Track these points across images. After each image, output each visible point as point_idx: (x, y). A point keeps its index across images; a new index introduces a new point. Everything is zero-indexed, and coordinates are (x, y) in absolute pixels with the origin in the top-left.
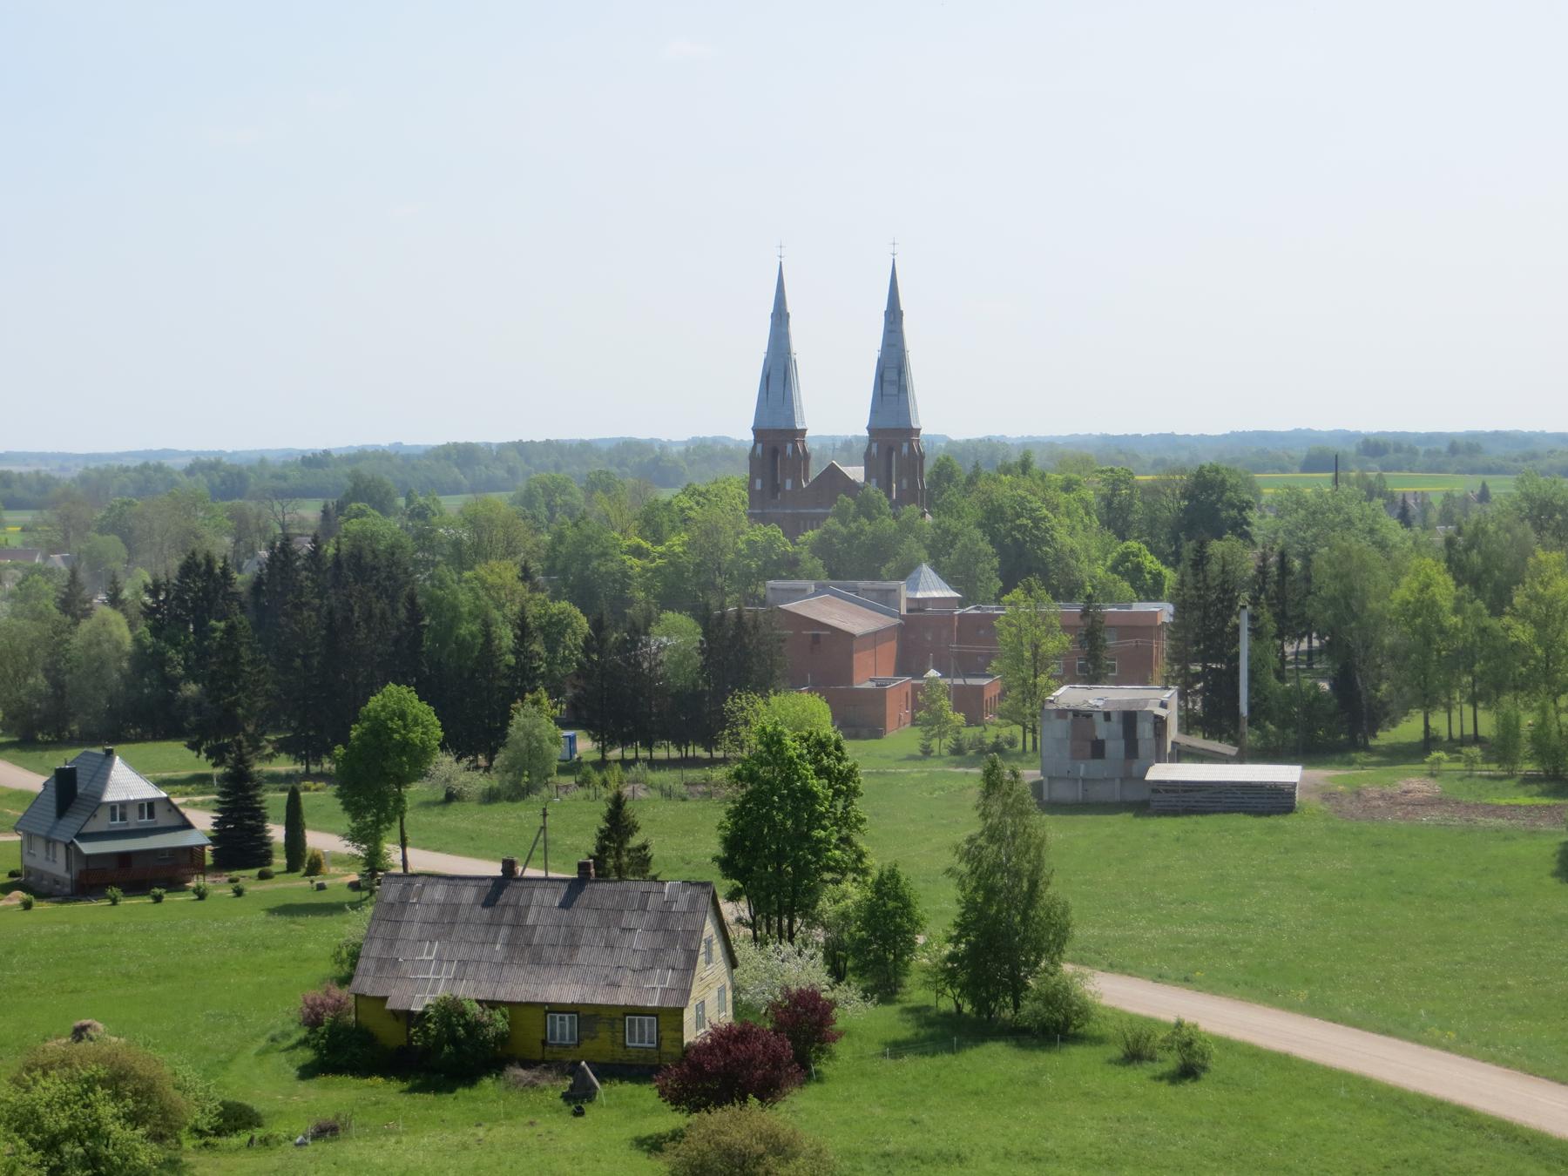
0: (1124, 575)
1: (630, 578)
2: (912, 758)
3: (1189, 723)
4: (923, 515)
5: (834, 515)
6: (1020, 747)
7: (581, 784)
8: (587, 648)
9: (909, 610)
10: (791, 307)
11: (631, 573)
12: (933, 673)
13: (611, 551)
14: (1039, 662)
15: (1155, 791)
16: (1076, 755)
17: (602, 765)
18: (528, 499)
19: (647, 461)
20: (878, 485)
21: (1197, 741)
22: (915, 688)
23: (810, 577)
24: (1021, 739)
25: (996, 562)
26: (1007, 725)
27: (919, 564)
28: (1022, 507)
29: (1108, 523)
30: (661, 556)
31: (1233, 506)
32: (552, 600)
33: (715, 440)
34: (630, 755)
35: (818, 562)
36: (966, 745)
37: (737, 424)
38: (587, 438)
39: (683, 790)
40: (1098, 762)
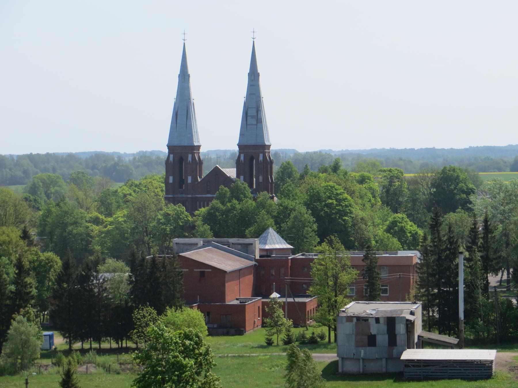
0: (394, 235)
1: (92, 237)
2: (262, 347)
3: (429, 324)
4: (272, 198)
5: (217, 198)
6: (327, 340)
7: (54, 364)
8: (60, 279)
9: (260, 257)
10: (191, 70)
11: (92, 234)
12: (275, 295)
13: (79, 221)
14: (338, 288)
15: (406, 366)
16: (359, 344)
17: (68, 352)
18: (33, 190)
19: (109, 166)
20: (245, 180)
21: (435, 336)
22: (264, 304)
23: (202, 236)
24: (327, 335)
25: (315, 227)
26: (320, 326)
27: (268, 227)
28: (331, 193)
29: (386, 202)
30: (111, 223)
31: (463, 192)
32: (43, 251)
33: (152, 153)
34: (86, 346)
35: (207, 227)
36: (294, 338)
37: (157, 141)
38: (74, 152)
39: (117, 367)
40: (373, 349)
